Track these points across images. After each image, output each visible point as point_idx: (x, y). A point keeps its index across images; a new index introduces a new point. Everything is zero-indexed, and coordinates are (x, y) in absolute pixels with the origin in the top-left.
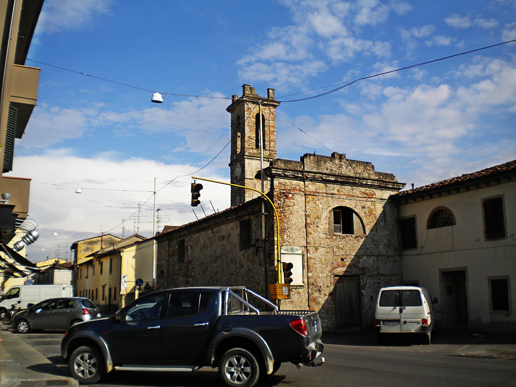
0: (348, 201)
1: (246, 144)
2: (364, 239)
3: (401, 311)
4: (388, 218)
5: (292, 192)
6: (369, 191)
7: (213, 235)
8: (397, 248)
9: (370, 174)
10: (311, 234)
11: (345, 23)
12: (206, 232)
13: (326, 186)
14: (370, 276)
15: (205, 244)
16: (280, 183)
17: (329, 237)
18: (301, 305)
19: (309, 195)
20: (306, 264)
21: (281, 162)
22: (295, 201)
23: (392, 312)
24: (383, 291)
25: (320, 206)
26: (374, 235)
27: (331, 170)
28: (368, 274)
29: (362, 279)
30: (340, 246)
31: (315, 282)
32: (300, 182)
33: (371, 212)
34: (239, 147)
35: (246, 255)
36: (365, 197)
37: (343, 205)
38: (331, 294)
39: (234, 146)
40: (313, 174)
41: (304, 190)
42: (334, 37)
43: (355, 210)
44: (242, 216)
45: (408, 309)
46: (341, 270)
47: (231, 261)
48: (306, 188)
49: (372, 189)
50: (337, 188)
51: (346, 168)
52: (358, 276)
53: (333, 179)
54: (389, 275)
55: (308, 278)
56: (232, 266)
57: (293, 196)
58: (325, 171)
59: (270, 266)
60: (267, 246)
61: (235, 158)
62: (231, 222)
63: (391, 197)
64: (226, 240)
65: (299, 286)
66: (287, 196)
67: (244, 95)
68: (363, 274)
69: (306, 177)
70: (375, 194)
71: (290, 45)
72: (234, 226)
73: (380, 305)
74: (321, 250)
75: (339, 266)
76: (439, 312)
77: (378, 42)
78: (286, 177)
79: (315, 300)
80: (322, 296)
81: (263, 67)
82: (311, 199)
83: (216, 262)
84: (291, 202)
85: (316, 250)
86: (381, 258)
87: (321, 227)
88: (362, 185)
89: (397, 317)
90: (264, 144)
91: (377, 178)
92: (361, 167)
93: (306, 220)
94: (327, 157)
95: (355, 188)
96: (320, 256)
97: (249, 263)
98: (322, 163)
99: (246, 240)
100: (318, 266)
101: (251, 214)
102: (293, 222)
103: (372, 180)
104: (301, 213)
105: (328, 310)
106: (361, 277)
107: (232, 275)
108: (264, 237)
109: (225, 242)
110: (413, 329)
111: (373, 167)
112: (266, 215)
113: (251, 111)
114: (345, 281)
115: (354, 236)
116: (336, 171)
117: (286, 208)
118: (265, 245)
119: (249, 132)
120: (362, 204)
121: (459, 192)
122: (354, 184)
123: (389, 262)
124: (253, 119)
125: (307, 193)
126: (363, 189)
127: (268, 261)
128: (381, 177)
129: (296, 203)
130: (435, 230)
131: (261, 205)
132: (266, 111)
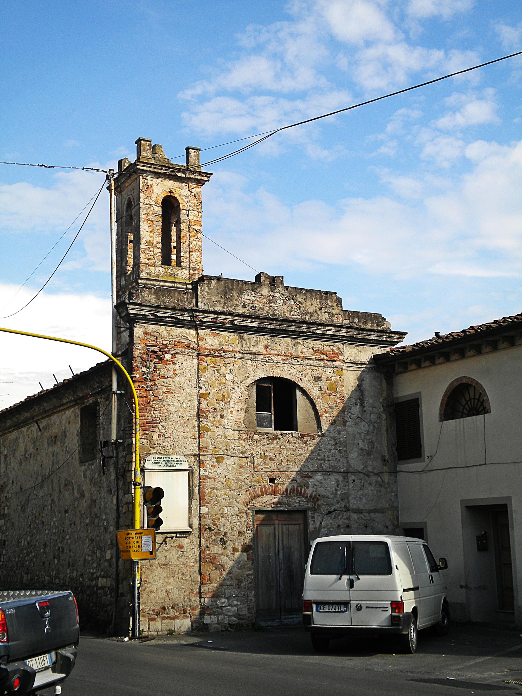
0: (285, 367)
1: (142, 255)
2: (317, 440)
3: (351, 584)
4: (369, 400)
5: (171, 351)
6: (329, 347)
7: (39, 433)
8: (387, 458)
9: (333, 315)
10: (208, 430)
11: (389, 15)
12: (29, 428)
13: (241, 338)
14: (330, 513)
15: (26, 451)
16: (146, 333)
18: (184, 571)
19: (206, 356)
20: (196, 489)
21: (150, 293)
22: (176, 367)
23: (334, 587)
24: (318, 544)
25: (229, 377)
26: (339, 433)
28: (324, 509)
29: (313, 517)
31: (215, 524)
32: (188, 331)
33: (332, 389)
34: (130, 261)
35: (88, 472)
38: (246, 549)
39: (122, 260)
40: (213, 315)
41: (195, 346)
42: (369, 43)
43: (300, 384)
44: (84, 398)
45: (365, 580)
46: (268, 501)
47: (66, 485)
48: (200, 343)
50: (265, 342)
51: (285, 303)
52: (304, 512)
54: (370, 512)
55: (200, 517)
56: (67, 494)
57: (173, 357)
58: (240, 310)
59: (125, 494)
60: (120, 455)
61: (123, 282)
62: (68, 408)
63: (376, 359)
64: (58, 443)
65: (181, 533)
66: (161, 359)
67: (138, 160)
68: (314, 510)
69: (200, 321)
71: (282, 60)
72: (73, 417)
73: (312, 573)
75: (264, 493)
76: (461, 587)
77: (454, 51)
78: (158, 321)
79: (213, 560)
80: (229, 552)
81: (230, 105)
82: (209, 362)
83: (42, 487)
84: (169, 370)
85: (218, 462)
86: (353, 477)
87: (229, 416)
88: (315, 336)
89: (344, 597)
90: (179, 257)
91: (346, 322)
92: (314, 302)
93: (199, 403)
94: (246, 283)
96: (225, 473)
97: (93, 489)
98: (235, 294)
99: (90, 443)
100: (220, 493)
101: (98, 393)
102: (172, 408)
103: (335, 326)
104: (188, 390)
105: (239, 581)
106: (310, 513)
107: (66, 512)
108: (114, 437)
109: (56, 449)
110: (378, 620)
111: (339, 301)
112: (120, 396)
113: (154, 191)
114: (277, 522)
115: (296, 434)
116: (263, 309)
117: (159, 382)
118: (117, 453)
119: (150, 233)
120: (315, 373)
121: (495, 348)
122: (298, 334)
123: (370, 484)
124: (156, 208)
125: (201, 352)
126: (317, 344)
127: (121, 483)
129: (178, 372)
130: (452, 422)
131: (111, 377)
132: (182, 192)
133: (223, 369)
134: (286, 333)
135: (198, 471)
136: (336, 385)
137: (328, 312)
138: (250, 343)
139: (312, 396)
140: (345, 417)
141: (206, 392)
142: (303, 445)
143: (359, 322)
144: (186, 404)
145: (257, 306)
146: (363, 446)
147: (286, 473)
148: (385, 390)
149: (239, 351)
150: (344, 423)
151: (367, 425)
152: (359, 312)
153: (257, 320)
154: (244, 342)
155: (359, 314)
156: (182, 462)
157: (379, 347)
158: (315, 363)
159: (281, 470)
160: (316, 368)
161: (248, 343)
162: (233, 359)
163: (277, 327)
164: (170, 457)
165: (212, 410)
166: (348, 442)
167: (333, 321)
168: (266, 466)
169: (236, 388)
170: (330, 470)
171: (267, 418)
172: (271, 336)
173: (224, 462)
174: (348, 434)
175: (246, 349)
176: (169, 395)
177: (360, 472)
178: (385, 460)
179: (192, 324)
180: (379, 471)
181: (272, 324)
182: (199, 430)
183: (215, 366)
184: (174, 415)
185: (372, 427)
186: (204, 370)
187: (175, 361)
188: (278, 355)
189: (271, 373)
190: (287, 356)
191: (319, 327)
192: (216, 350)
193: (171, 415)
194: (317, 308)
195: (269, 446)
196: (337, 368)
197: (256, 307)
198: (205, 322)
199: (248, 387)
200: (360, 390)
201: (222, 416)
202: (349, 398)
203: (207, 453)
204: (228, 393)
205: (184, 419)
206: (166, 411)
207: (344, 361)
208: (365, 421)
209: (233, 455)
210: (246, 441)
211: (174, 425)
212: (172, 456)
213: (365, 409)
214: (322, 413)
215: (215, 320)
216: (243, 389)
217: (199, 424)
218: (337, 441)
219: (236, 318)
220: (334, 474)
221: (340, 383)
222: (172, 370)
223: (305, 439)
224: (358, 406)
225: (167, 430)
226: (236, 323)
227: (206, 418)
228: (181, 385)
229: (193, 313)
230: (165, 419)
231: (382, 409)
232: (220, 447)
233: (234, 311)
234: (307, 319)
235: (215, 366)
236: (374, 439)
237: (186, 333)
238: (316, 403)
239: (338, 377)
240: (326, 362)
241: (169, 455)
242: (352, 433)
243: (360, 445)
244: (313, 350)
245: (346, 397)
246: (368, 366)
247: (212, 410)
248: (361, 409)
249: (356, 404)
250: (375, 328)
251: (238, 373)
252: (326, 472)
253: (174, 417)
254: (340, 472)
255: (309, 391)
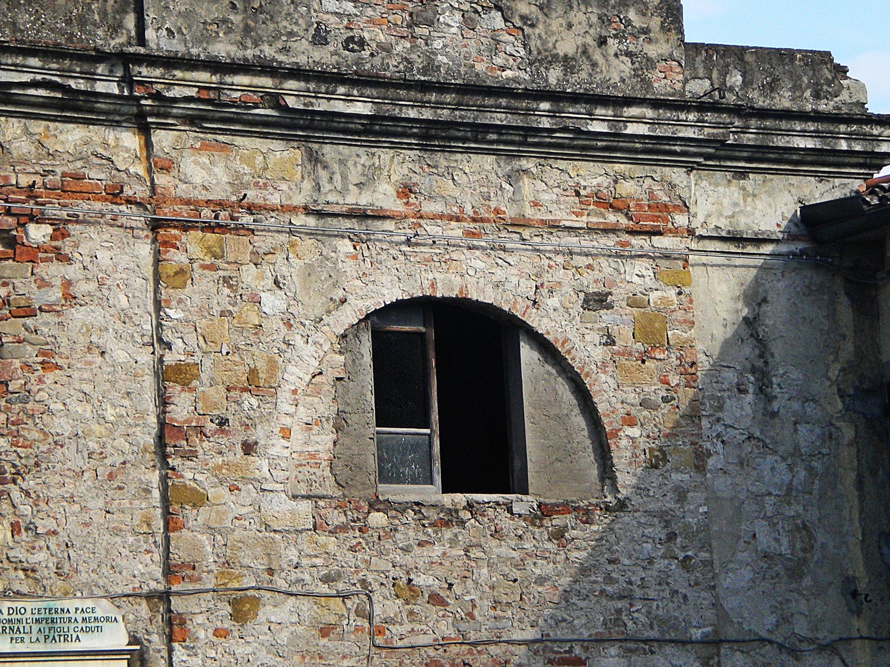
0: (477, 261)
4: (787, 374)
5: (52, 211)
6: (635, 183)
8: (862, 586)
9: (650, 63)
10: (199, 499)
13: (314, 159)
17: (337, 518)
19: (186, 226)
22: (72, 271)
25: (273, 302)
26: (681, 495)
27: (355, 43)
30: (420, 580)
32: (111, 135)
33: (652, 334)
36: (608, 230)
37: (445, 284)
40: (203, 76)
41: (140, 191)
48: (161, 180)
49: (659, 172)
51: (468, 23)
53: (362, 108)
57: (60, 233)
58: (305, 54)
63: (811, 219)
69: (157, 96)
70: (685, 207)
74: (276, 613)
82: (195, 250)
84: (43, 284)
88: (584, 146)
91: (699, 87)
92: (578, 17)
93: (163, 401)
95: (527, 164)
102: (61, 425)
103: (656, 104)
104: (120, 356)
115: (523, 504)
116: (387, 49)
122: (520, 141)
125: (167, 212)
126: (592, 175)
128: (736, 79)
129: (81, 288)
133: (249, 275)
134: (474, 138)
135: (165, 654)
136: (664, 321)
137: (629, 54)
138: (344, 177)
139: (576, 365)
140: (699, 436)
141: (190, 360)
142: (549, 546)
143: (746, 84)
144: (114, 406)
145: (366, 35)
146: (773, 544)
147: (493, 649)
148: (849, 333)
149: (306, 208)
150: (700, 460)
151: (783, 466)
152: (744, 49)
153: (368, 91)
154: (323, 174)
155: (748, 58)
156: (105, 625)
157: (822, 177)
158: (586, 242)
159: (473, 637)
160: (589, 261)
161: (337, 177)
162: (284, 238)
163: (445, 114)
164: (59, 604)
165: (210, 427)
166: (715, 528)
167: (647, 84)
168: (417, 627)
169: (299, 341)
170: (654, 634)
171: (415, 447)
172: (423, 148)
173: (261, 617)
174: (712, 498)
175: (332, 198)
176: (50, 377)
177: (762, 640)
178: (855, 594)
179: (125, 109)
180: (835, 637)
181: (423, 105)
182: (166, 501)
183: (219, 262)
184: (69, 451)
185: (802, 474)
186: (178, 281)
187: (67, 250)
188: (451, 218)
189: (426, 284)
190: (482, 220)
191: (600, 111)
192: (221, 204)
193: (59, 451)
194: (589, 40)
195: (426, 551)
196: (667, 257)
197: (362, 43)
198: (175, 100)
199: (344, 336)
200: (754, 336)
201: (249, 448)
202: (717, 368)
203: (198, 586)
204: (272, 365)
205: (108, 461)
206: (36, 435)
207: (691, 232)
208: (774, 452)
209: (293, 589)
210: (342, 536)
211: (70, 487)
212: (66, 604)
213: (775, 405)
214: (615, 425)
215: (212, 95)
216: (326, 347)
217: (164, 479)
218: (676, 528)
219: (291, 84)
220: (669, 649)
221: (679, 315)
222: (58, 282)
223: (558, 520)
224: (750, 397)
225: (43, 505)
226: (291, 102)
227: (190, 455)
228: (94, 339)
229: (127, 69)
230: (37, 464)
231: (840, 406)
232: (246, 561)
233: (281, 58)
234: (553, 81)
235: (219, 262)
236: (813, 515)
237: (105, 144)
238: (593, 389)
239: (672, 293)
240: (626, 237)
241: (54, 597)
242: (727, 495)
243: (760, 537)
244: (578, 194)
245: (704, 363)
246: (784, 248)
247: (210, 427)
248: (761, 405)
249: (742, 391)
250: (809, 107)
251: (306, 289)
252: (636, 641)
253: (71, 457)
254: (691, 642)
255: (567, 346)
